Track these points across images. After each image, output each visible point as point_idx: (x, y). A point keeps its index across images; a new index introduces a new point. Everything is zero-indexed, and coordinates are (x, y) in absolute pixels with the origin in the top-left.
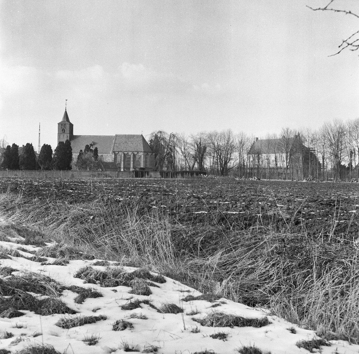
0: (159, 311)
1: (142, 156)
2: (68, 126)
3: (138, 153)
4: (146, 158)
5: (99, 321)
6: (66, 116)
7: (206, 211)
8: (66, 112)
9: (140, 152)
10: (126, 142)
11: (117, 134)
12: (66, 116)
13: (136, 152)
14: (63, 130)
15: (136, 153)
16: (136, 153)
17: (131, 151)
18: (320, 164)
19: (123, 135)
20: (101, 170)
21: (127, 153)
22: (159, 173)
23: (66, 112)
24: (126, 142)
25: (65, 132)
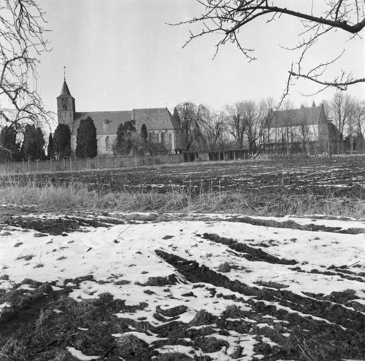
0: (310, 273)
1: (173, 134)
2: (70, 101)
3: (166, 131)
4: (176, 136)
5: (210, 357)
6: (66, 87)
7: (79, 330)
8: (65, 83)
9: (169, 129)
10: (148, 118)
11: (135, 108)
12: (66, 87)
13: (163, 129)
14: (64, 106)
15: (164, 131)
16: (164, 131)
17: (157, 128)
18: (93, 220)
19: (143, 109)
20: (148, 154)
21: (152, 131)
22: (207, 155)
23: (65, 83)
24: (148, 118)
25: (68, 108)
